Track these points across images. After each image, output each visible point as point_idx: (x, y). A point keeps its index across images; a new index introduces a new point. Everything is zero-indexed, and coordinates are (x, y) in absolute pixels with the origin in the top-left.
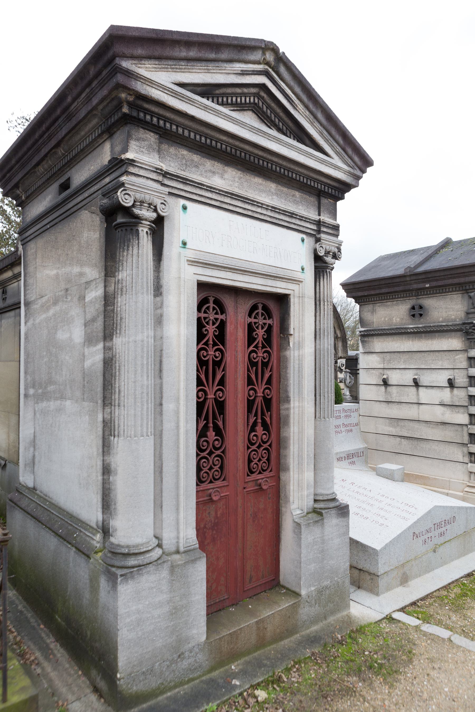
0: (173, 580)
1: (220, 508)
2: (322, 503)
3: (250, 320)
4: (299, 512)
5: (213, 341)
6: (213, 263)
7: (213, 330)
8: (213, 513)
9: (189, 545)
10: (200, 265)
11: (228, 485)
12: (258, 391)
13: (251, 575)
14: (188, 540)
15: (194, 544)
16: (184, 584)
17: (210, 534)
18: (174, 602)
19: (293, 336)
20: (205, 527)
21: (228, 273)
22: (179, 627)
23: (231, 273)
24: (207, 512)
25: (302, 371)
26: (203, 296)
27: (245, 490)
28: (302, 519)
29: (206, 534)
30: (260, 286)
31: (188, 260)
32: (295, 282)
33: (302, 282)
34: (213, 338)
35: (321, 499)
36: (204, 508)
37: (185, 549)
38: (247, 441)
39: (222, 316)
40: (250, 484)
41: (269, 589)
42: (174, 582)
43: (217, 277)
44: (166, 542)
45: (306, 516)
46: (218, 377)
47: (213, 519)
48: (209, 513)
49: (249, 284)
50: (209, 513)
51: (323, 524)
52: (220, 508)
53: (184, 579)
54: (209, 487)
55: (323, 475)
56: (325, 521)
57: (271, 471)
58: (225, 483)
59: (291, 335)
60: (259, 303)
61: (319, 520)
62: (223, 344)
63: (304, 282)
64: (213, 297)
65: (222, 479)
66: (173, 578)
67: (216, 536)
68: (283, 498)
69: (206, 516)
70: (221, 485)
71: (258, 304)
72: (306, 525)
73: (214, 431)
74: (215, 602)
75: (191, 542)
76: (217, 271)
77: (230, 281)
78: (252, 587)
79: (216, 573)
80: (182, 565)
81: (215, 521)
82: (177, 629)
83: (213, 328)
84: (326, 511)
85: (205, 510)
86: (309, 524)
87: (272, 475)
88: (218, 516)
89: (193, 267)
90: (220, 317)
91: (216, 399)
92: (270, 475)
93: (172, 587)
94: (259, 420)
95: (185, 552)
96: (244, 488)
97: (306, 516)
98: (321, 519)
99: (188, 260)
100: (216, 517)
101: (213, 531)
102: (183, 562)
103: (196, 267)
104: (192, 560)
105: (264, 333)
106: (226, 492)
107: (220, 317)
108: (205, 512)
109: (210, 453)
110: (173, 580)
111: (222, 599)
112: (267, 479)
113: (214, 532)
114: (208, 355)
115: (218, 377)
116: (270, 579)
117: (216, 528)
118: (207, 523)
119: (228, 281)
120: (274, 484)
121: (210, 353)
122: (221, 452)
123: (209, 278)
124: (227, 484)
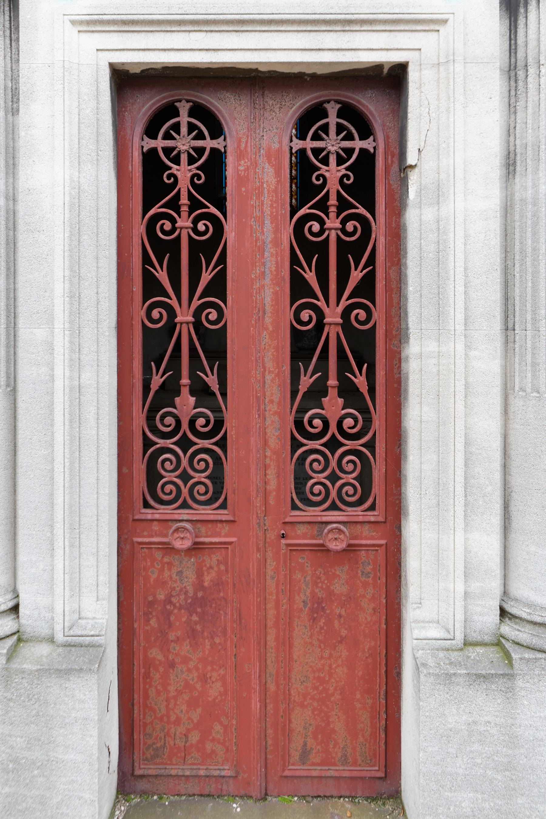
0: (10, 700)
1: (211, 567)
2: (528, 628)
3: (298, 144)
4: (434, 632)
5: (191, 196)
6: (142, 17)
7: (189, 175)
8: (190, 576)
9: (79, 633)
10: (112, 28)
11: (234, 521)
12: (326, 310)
13: (305, 744)
14: (83, 622)
15: (92, 633)
16: (37, 715)
17: (184, 619)
18: (12, 747)
19: (416, 170)
20: (168, 600)
21: (193, 35)
22: (24, 805)
23: (204, 34)
24: (174, 570)
25: (71, 235)
26: (158, 101)
27: (283, 541)
28: (441, 654)
29: (172, 618)
30: (298, 53)
31: (73, 22)
32: (419, 27)
33: (445, 21)
34: (189, 191)
35: (524, 615)
36: (166, 560)
37: (69, 639)
38: (291, 424)
39: (214, 142)
40: (301, 529)
41: (367, 798)
42: (11, 704)
43: (165, 50)
44: (27, 612)
45: (461, 650)
46: (206, 277)
47: (190, 589)
48: (181, 572)
49: (262, 53)
50: (181, 572)
51: (511, 690)
52: (211, 567)
53: (36, 706)
54: (176, 517)
55: (533, 549)
56: (520, 683)
57: (372, 508)
58: (224, 515)
59: (412, 167)
60: (328, 102)
61: (496, 675)
62: (221, 205)
63: (450, 22)
64: (188, 101)
65: (217, 504)
66: (8, 695)
67: (198, 627)
68: (404, 586)
69: (171, 577)
70: (212, 518)
71: (326, 105)
72: (437, 675)
73: (340, 396)
74: (194, 773)
75: (89, 626)
76: (162, 34)
77: (203, 53)
78: (305, 774)
79: (199, 710)
80: (31, 672)
81: (195, 593)
82: (20, 808)
83: (190, 170)
84: (528, 655)
85: (170, 564)
86: (449, 676)
87: (372, 519)
88: (206, 584)
89: (96, 35)
90: (209, 143)
91: (197, 325)
92: (366, 519)
93: (7, 712)
94: (333, 382)
95: (67, 645)
96: (283, 536)
97: (461, 650)
98: (504, 675)
99: (73, 22)
100: (199, 585)
101: (191, 615)
102: (35, 668)
103: (104, 34)
104: (58, 671)
105: (344, 172)
106: (226, 536)
107: (209, 143)
108: (170, 569)
109: (333, 445)
110: (10, 700)
111: (216, 773)
112: (342, 527)
113: (195, 618)
114: (174, 229)
115: (206, 277)
116: (368, 775)
117: (199, 610)
118: (174, 593)
119: (197, 53)
120: (383, 542)
121: (179, 223)
122: (215, 444)
123: (141, 54)
124: (230, 518)
